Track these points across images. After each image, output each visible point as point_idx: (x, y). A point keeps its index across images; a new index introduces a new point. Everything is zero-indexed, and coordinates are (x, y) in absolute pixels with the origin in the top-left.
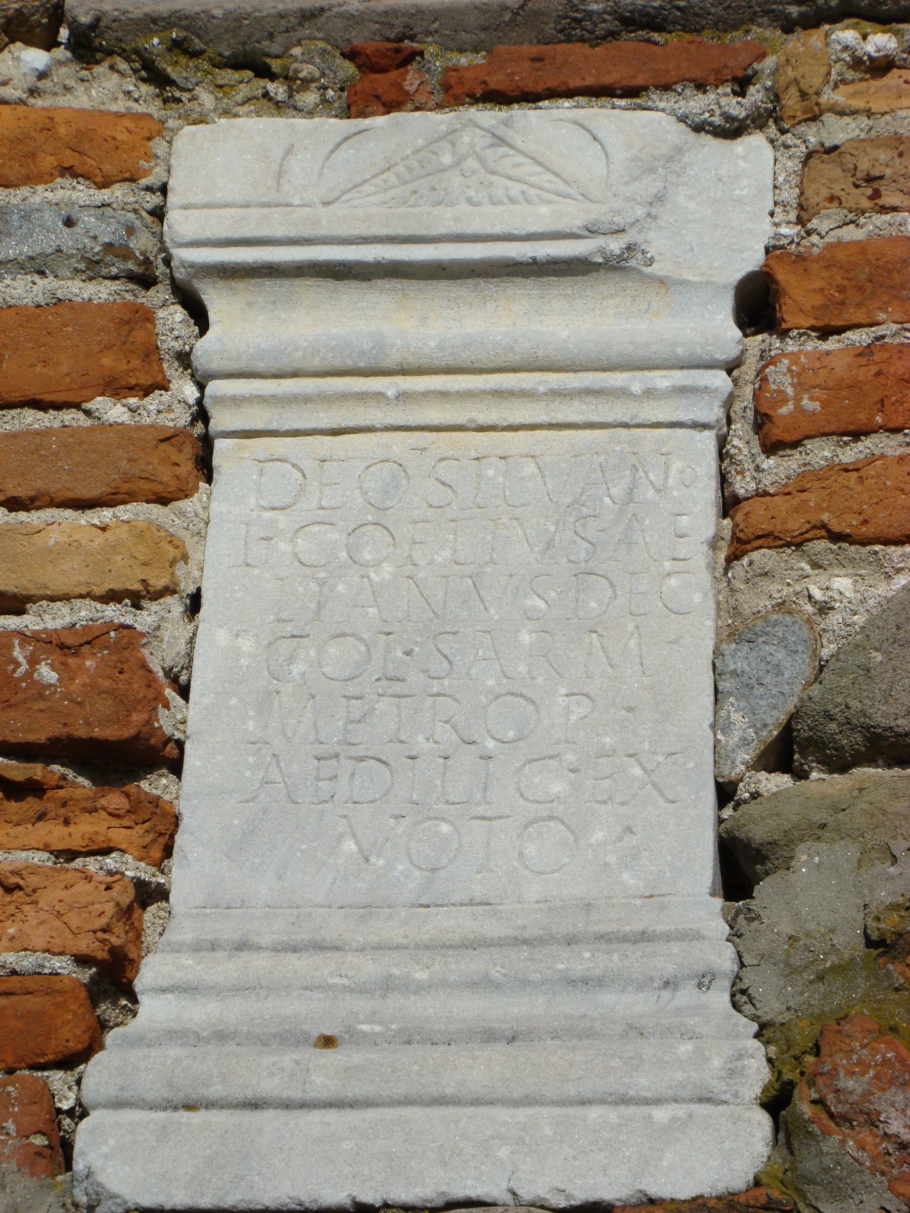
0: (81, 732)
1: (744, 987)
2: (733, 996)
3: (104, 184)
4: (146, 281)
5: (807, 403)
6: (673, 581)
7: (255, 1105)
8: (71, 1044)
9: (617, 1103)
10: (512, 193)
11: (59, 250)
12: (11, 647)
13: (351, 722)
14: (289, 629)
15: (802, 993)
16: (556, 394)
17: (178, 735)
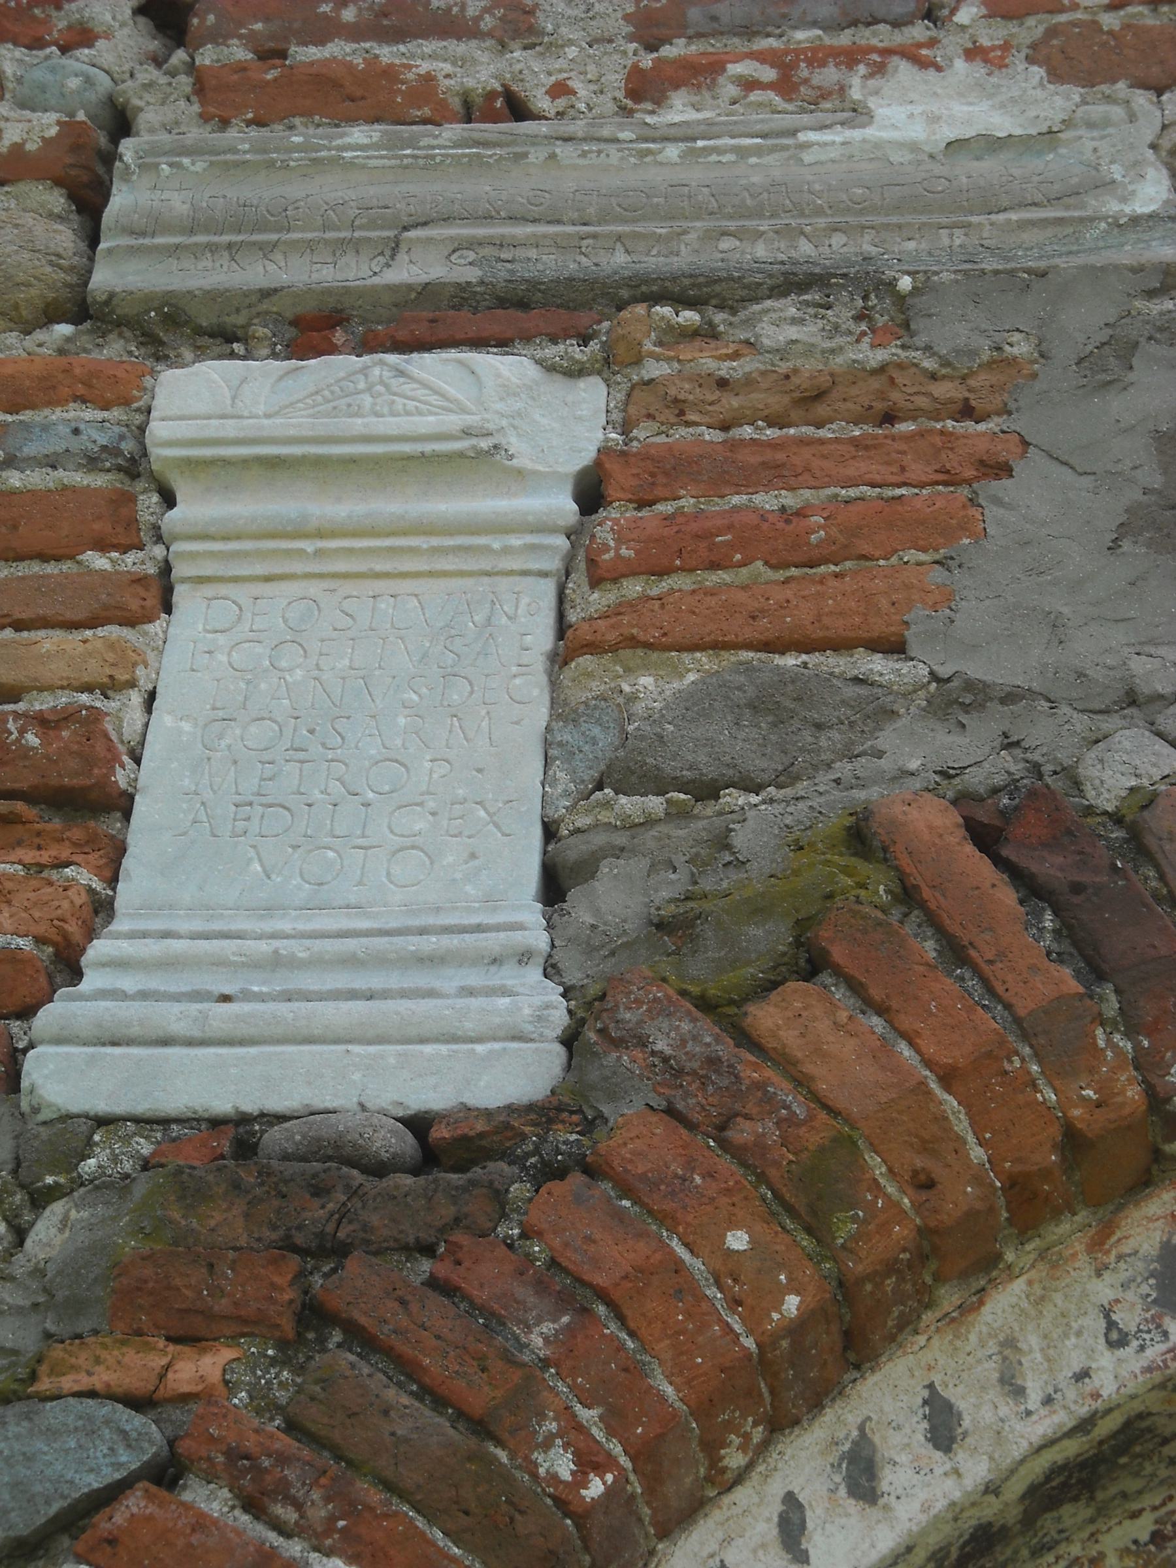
0: (54, 781)
1: (553, 961)
2: (545, 970)
3: (105, 408)
4: (134, 476)
5: (624, 552)
6: (517, 681)
7: (166, 1042)
8: (28, 999)
9: (447, 1042)
10: (408, 408)
11: (67, 451)
12: (6, 721)
13: (264, 780)
14: (221, 714)
15: (599, 965)
16: (435, 551)
17: (130, 790)
